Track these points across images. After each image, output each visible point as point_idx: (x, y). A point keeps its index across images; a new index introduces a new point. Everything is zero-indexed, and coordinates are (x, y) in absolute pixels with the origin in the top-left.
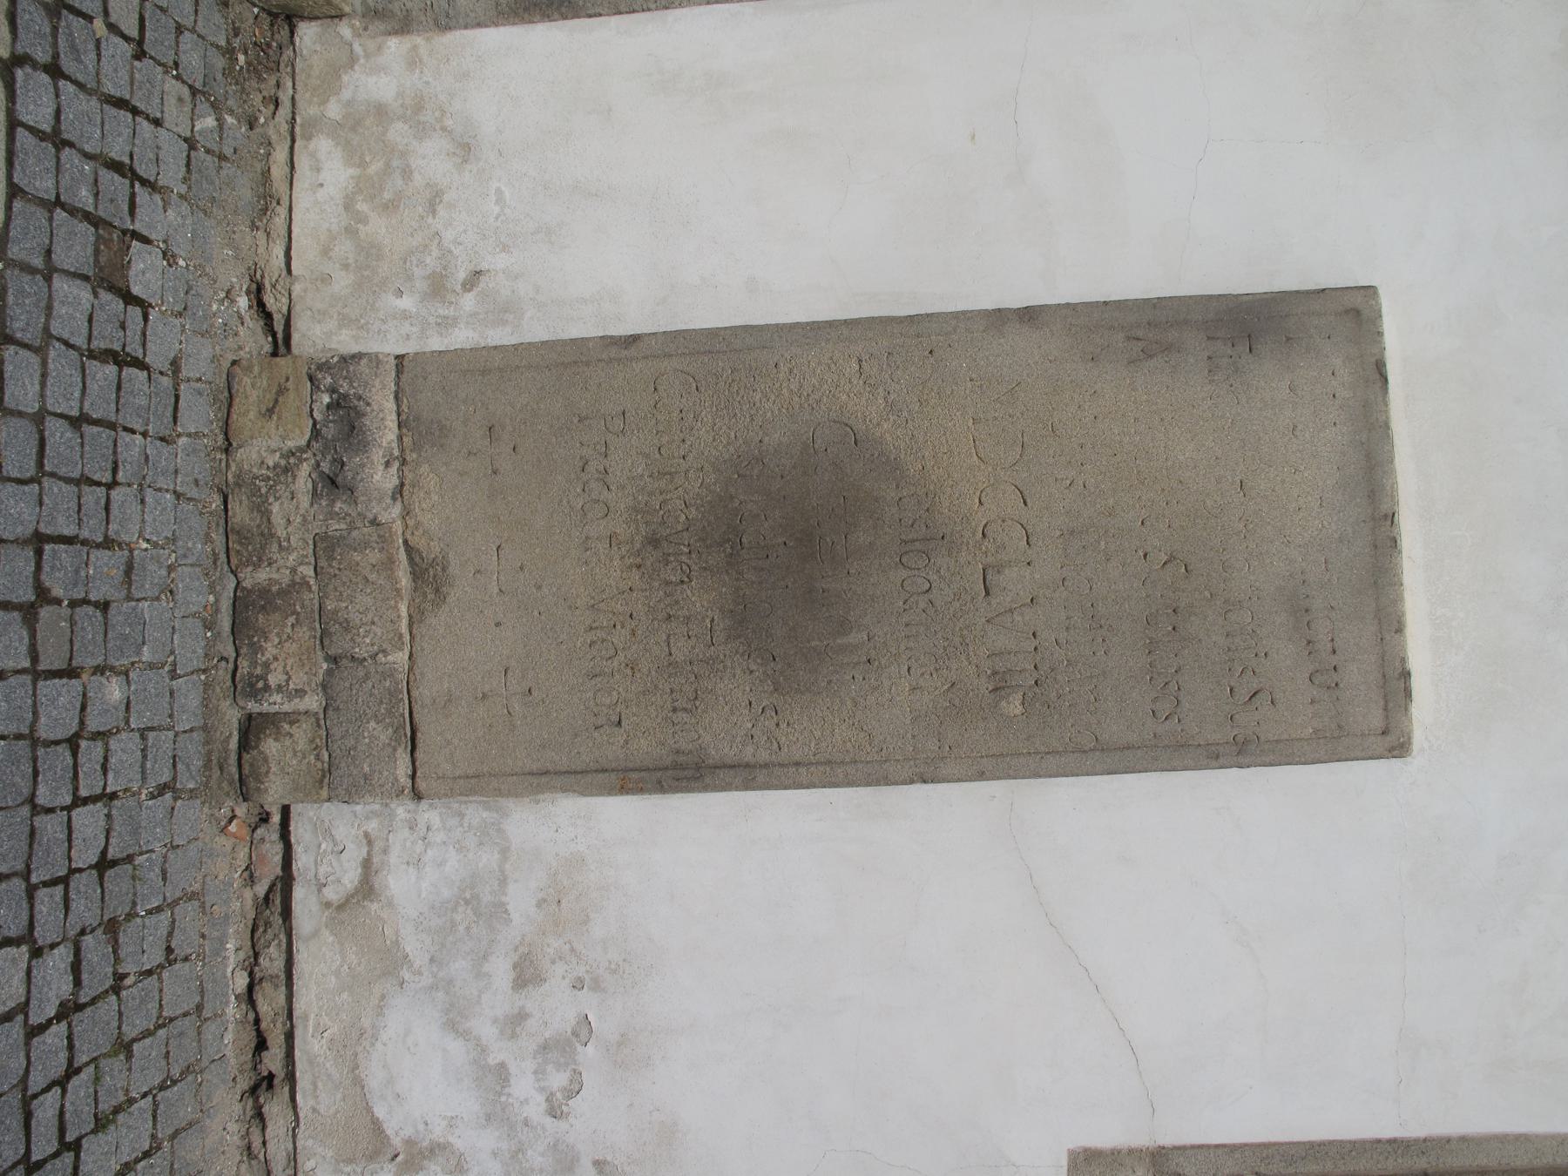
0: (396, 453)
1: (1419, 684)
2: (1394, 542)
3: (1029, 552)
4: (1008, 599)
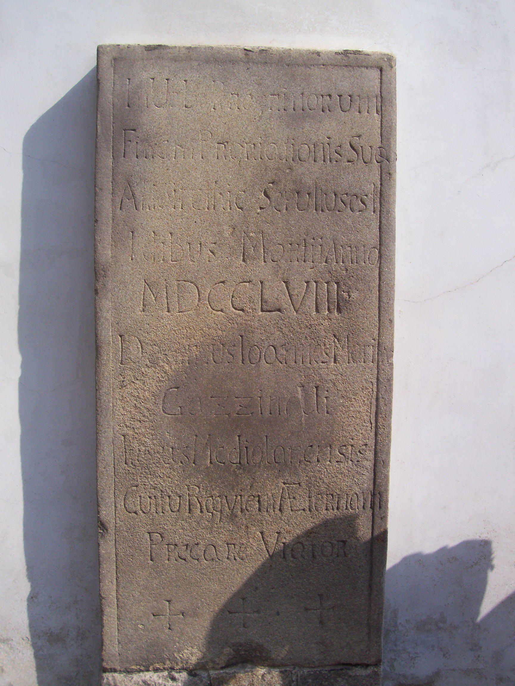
0: (166, 673)
1: (351, 46)
2: (262, 51)
3: (254, 281)
4: (283, 297)
